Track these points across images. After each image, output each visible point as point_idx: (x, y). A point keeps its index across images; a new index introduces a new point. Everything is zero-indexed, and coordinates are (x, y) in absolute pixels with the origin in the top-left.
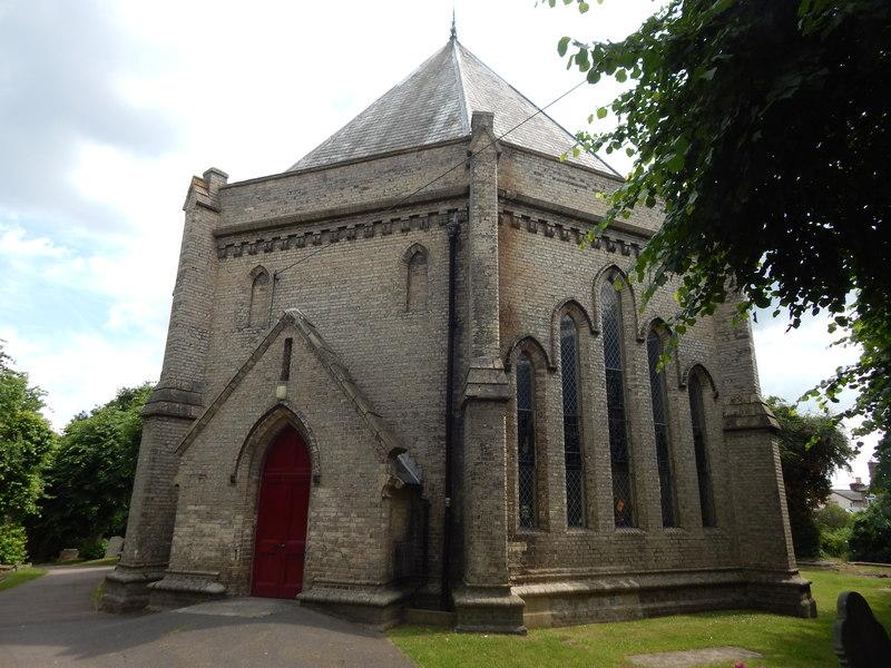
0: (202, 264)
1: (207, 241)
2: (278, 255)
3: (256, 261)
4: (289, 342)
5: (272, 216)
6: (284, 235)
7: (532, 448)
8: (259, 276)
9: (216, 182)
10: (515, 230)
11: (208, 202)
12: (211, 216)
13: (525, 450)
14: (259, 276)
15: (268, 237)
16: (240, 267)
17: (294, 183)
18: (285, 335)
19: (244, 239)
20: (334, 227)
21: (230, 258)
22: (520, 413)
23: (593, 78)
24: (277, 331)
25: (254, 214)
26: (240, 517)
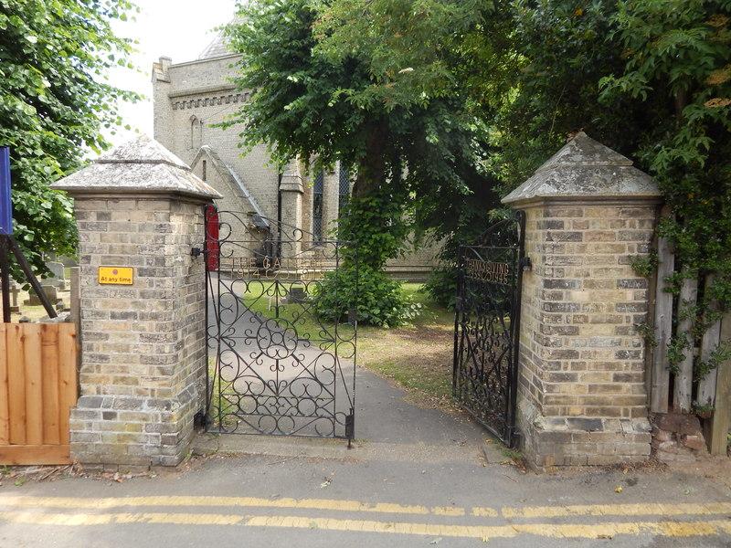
0: (165, 114)
1: (166, 100)
2: (201, 108)
3: (193, 112)
4: (204, 161)
5: (196, 87)
6: (203, 98)
7: (321, 210)
8: (194, 121)
9: (166, 64)
10: (597, 432)
11: (163, 78)
12: (166, 85)
13: (318, 211)
14: (194, 121)
15: (196, 99)
16: (184, 115)
17: (204, 67)
18: (202, 159)
19: (184, 99)
20: (227, 95)
21: (179, 110)
22: (315, 195)
23: (61, 300)
24: (199, 157)
25: (188, 85)
26: (296, 80)
